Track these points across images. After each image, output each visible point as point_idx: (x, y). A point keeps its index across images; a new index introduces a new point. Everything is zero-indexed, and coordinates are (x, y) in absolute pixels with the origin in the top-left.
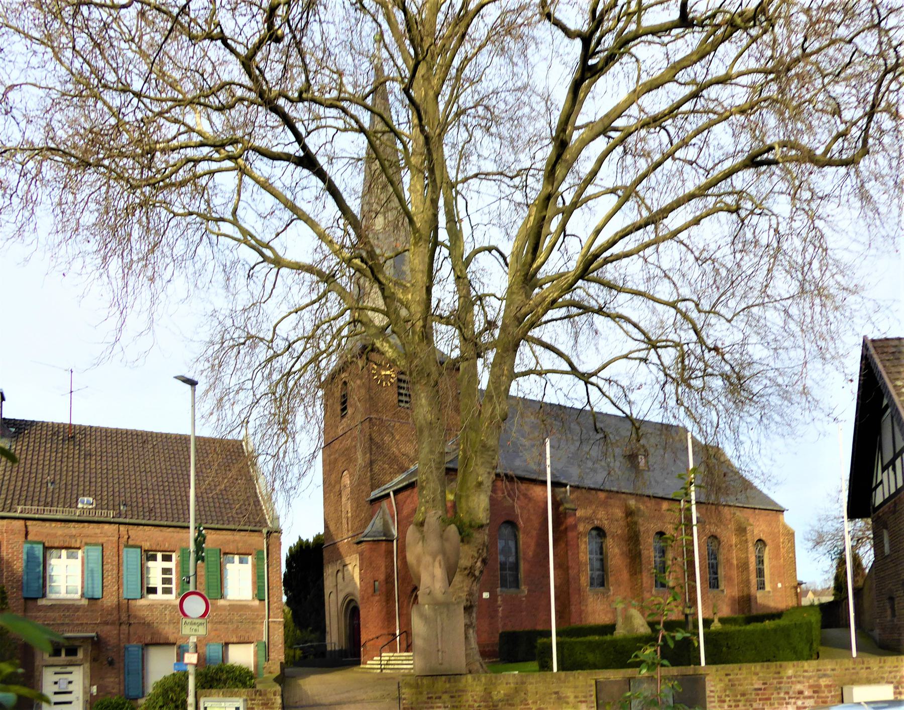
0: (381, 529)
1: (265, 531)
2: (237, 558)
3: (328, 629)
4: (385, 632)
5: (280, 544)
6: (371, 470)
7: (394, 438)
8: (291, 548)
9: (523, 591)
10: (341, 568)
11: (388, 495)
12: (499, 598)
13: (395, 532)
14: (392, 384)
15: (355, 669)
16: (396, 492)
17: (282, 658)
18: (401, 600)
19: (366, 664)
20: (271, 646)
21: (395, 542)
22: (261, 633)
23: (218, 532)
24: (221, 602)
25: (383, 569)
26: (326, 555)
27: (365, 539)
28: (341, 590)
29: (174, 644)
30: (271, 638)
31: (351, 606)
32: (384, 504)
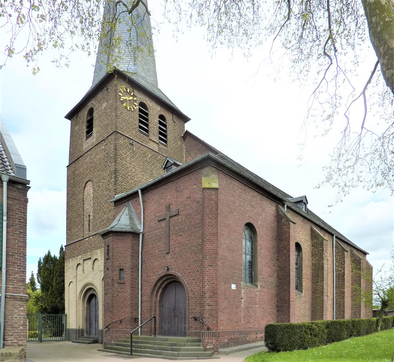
5: (26, 201)
6: (116, 177)
10: (81, 262)
11: (137, 193)
28: (81, 280)
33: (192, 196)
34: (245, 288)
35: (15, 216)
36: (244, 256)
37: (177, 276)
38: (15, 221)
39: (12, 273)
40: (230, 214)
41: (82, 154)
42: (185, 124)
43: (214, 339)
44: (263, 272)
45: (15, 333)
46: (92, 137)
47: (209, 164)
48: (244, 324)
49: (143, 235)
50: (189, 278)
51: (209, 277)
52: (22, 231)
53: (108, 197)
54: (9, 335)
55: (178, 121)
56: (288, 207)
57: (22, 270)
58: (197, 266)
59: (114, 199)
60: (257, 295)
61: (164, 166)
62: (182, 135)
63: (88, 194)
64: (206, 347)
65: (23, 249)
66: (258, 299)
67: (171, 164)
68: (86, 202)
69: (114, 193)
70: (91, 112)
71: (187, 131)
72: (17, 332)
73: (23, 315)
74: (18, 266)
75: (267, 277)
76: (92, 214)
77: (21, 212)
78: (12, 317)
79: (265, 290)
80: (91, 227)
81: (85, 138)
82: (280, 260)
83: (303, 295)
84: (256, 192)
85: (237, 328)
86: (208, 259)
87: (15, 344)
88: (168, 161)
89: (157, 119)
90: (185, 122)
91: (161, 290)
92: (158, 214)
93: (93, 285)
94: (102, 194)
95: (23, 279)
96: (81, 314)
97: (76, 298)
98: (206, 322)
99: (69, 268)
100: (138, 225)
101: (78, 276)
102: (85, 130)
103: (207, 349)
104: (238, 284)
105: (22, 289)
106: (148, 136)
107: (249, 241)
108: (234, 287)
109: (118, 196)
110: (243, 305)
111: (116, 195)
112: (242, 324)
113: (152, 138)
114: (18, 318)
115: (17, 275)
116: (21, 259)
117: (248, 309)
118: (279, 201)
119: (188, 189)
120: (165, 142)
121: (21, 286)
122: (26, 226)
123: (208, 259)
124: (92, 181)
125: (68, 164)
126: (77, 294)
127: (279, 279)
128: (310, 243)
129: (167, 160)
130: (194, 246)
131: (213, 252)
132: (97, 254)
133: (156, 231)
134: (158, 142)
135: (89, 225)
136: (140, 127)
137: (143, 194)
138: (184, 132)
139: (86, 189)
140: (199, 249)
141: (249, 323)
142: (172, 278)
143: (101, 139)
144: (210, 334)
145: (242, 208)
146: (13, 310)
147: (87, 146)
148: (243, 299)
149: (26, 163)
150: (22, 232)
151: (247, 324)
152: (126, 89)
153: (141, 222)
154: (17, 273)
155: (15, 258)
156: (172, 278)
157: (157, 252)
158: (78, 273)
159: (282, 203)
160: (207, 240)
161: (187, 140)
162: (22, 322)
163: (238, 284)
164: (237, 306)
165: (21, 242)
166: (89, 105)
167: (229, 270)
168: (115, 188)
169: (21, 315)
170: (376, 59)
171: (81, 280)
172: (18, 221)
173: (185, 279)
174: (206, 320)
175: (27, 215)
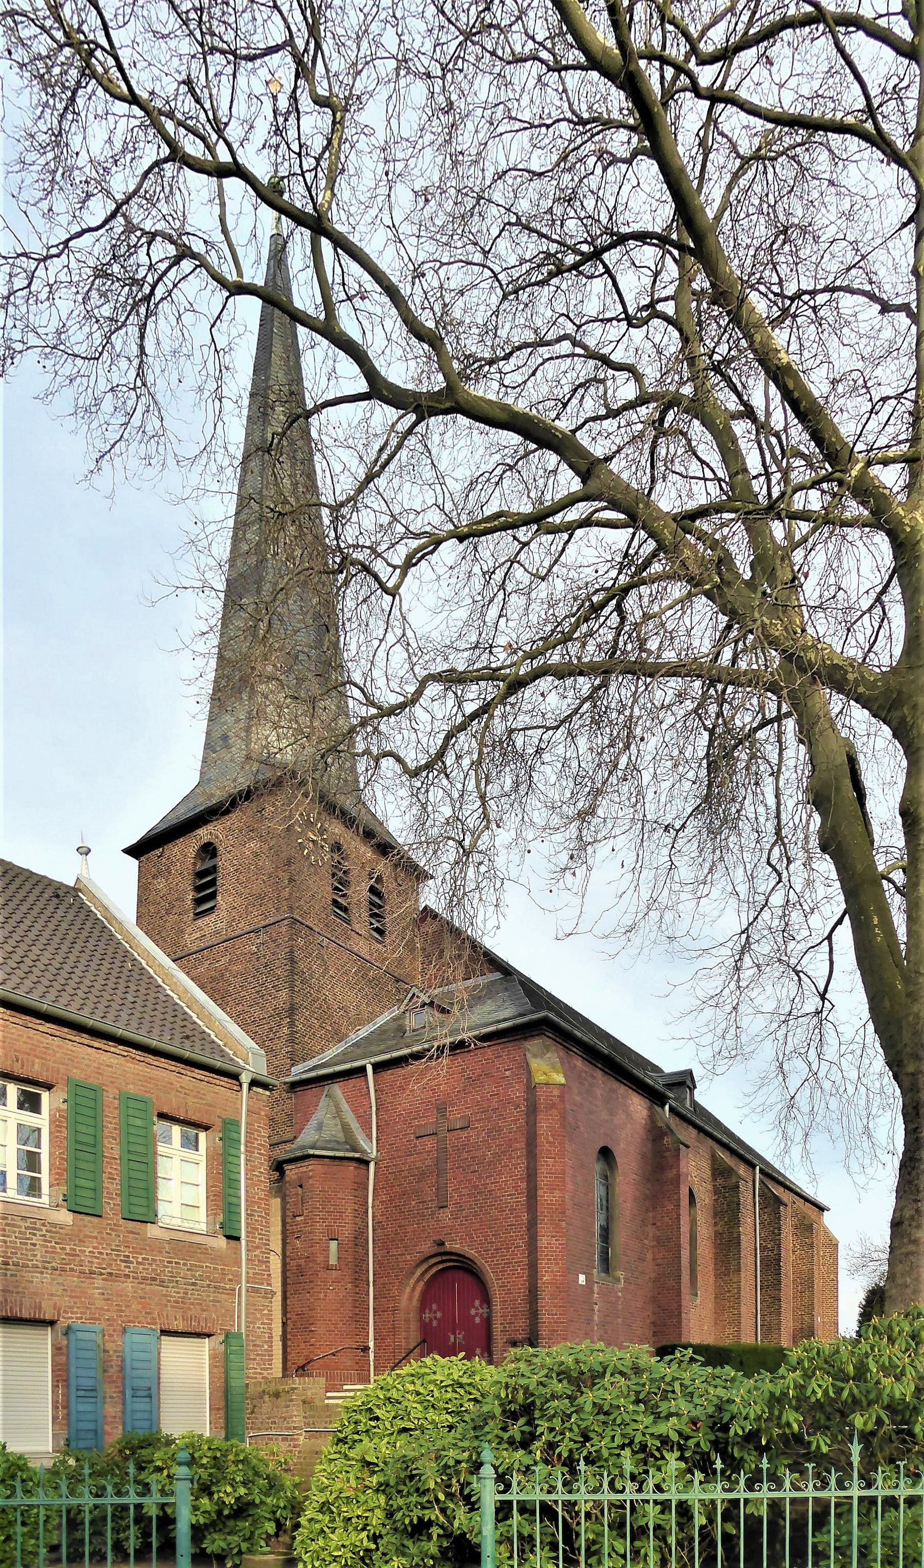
0: (341, 1136)
2: (176, 1130)
6: (292, 1024)
9: (618, 1280)
11: (363, 1069)
12: (596, 1288)
13: (371, 1149)
16: (377, 1067)
21: (372, 1165)
22: (230, 1313)
23: (150, 1059)
24: (152, 1231)
29: (52, 1323)
46: (214, 915)
56: (672, 1109)
60: (619, 1297)
82: (659, 1224)
83: (698, 1301)
91: (421, 1284)
106: (348, 922)
108: (582, 1279)
110: (596, 1318)
111: (293, 1065)
113: (357, 927)
128: (710, 1187)
137: (375, 1071)
154: (257, 1247)
170: (843, 906)
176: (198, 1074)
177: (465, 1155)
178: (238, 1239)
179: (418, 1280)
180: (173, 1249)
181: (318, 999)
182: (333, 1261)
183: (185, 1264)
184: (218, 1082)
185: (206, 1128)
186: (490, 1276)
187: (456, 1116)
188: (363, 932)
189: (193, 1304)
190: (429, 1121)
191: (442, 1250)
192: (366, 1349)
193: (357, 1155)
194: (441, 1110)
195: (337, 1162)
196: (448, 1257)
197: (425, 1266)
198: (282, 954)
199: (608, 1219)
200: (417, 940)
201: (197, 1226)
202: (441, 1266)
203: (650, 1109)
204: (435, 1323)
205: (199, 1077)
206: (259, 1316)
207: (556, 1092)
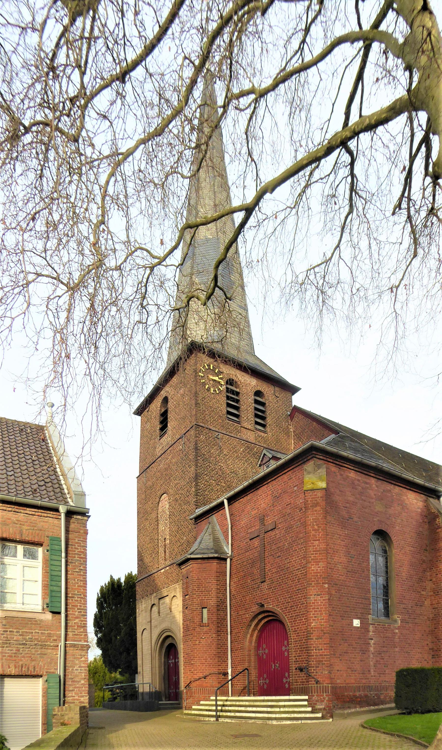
0: (211, 545)
1: (63, 509)
2: (20, 548)
3: (139, 669)
4: (215, 670)
5: (86, 533)
6: (197, 485)
7: (221, 451)
8: (102, 587)
9: (396, 621)
10: (156, 602)
11: (222, 504)
12: (371, 628)
13: (228, 550)
14: (221, 391)
15: (177, 714)
17: (85, 700)
18: (234, 632)
19: (190, 708)
20: (69, 683)
21: (228, 560)
25: (214, 593)
26: (139, 589)
27: (192, 556)
28: (156, 626)
30: (69, 670)
31: (166, 644)
32: (214, 518)
33: (292, 502)
34: (375, 624)
35: (75, 551)
36: (372, 579)
37: (276, 612)
38: (75, 557)
39: (72, 617)
40: (348, 520)
41: (155, 459)
42: (293, 397)
43: (326, 695)
44: (405, 599)
45: (75, 687)
47: (313, 455)
48: (375, 676)
49: (231, 560)
50: (292, 614)
51: (317, 611)
52: (82, 568)
53: (187, 513)
54: (70, 691)
55: (282, 394)
57: (82, 613)
58: (302, 597)
59: (194, 515)
61: (259, 463)
62: (289, 413)
63: (163, 511)
64: (314, 707)
65: (83, 589)
66: (398, 640)
67: (268, 459)
68: (161, 522)
69: (194, 507)
70: (166, 400)
71: (295, 406)
72: (78, 687)
73: (84, 667)
74: (78, 609)
75: (412, 607)
76: (168, 537)
77: (80, 546)
78: (73, 670)
79: (410, 625)
80: (167, 554)
81: (159, 438)
82: (434, 579)
84: (390, 484)
85: (364, 681)
86: (314, 586)
87: (76, 701)
88: (265, 454)
89: (251, 399)
90: (293, 394)
92: (250, 531)
93: (172, 632)
94: (180, 509)
95: (84, 624)
96: (157, 672)
97: (151, 650)
98: (314, 673)
99: (142, 611)
100: (225, 547)
101: (152, 621)
102: (159, 427)
103: (316, 710)
104: (364, 618)
105: (83, 636)
106: (239, 423)
107: (383, 556)
108: (356, 623)
109: (199, 511)
110: (372, 649)
112: (372, 676)
113: (245, 425)
114: (79, 671)
115: (77, 621)
116: (81, 601)
117: (380, 654)
118: (429, 493)
119: (287, 492)
120: (264, 426)
121: (81, 632)
122: (86, 562)
123: (314, 586)
124: (167, 494)
125: (138, 474)
126: (151, 646)
127: (433, 609)
129: (263, 454)
130: (297, 570)
131: (321, 576)
132: (175, 589)
133: (247, 554)
134: (253, 428)
135: (165, 552)
136: (229, 413)
137: (229, 504)
138: (291, 408)
139: (160, 504)
140: (303, 573)
141: (383, 674)
142: (276, 617)
143: (178, 436)
144: (320, 689)
145: (366, 510)
146: (73, 661)
147: (161, 447)
148: (372, 639)
149: (86, 489)
150: (81, 570)
151: (380, 676)
152: (209, 366)
153: (228, 543)
154: (77, 618)
155: (75, 600)
156: (276, 617)
157: (249, 581)
158: (152, 617)
159: (435, 495)
160: (312, 559)
161: (295, 419)
162: (83, 674)
163: (364, 618)
164: (363, 651)
165: (81, 581)
166: (163, 393)
167: (348, 599)
168: (195, 499)
169: (82, 667)
171: (156, 626)
172: (78, 557)
173: (286, 615)
174: (314, 670)
175: (87, 549)
176: (29, 511)
177: (274, 547)
178: (59, 613)
179: (254, 630)
180: (8, 622)
181: (215, 469)
182: (205, 620)
183: (17, 632)
184: (45, 515)
185: (41, 545)
186: (288, 624)
187: (269, 521)
188: (250, 427)
189: (23, 657)
190: (256, 528)
191: (262, 609)
192: (226, 674)
193: (216, 555)
194: (262, 520)
195: (206, 561)
196: (268, 614)
197: (256, 621)
198: (192, 446)
199: (387, 580)
200: (290, 427)
201: (37, 607)
202: (266, 620)
203: (426, 501)
204: (265, 657)
205: (30, 513)
206: (77, 662)
207: (319, 494)
